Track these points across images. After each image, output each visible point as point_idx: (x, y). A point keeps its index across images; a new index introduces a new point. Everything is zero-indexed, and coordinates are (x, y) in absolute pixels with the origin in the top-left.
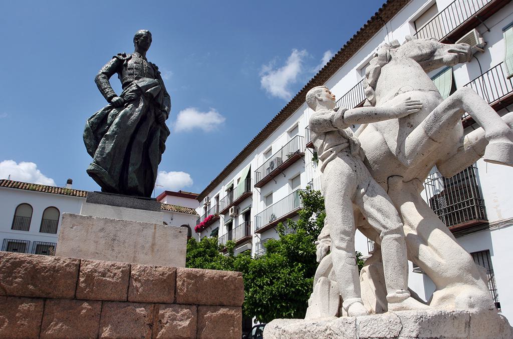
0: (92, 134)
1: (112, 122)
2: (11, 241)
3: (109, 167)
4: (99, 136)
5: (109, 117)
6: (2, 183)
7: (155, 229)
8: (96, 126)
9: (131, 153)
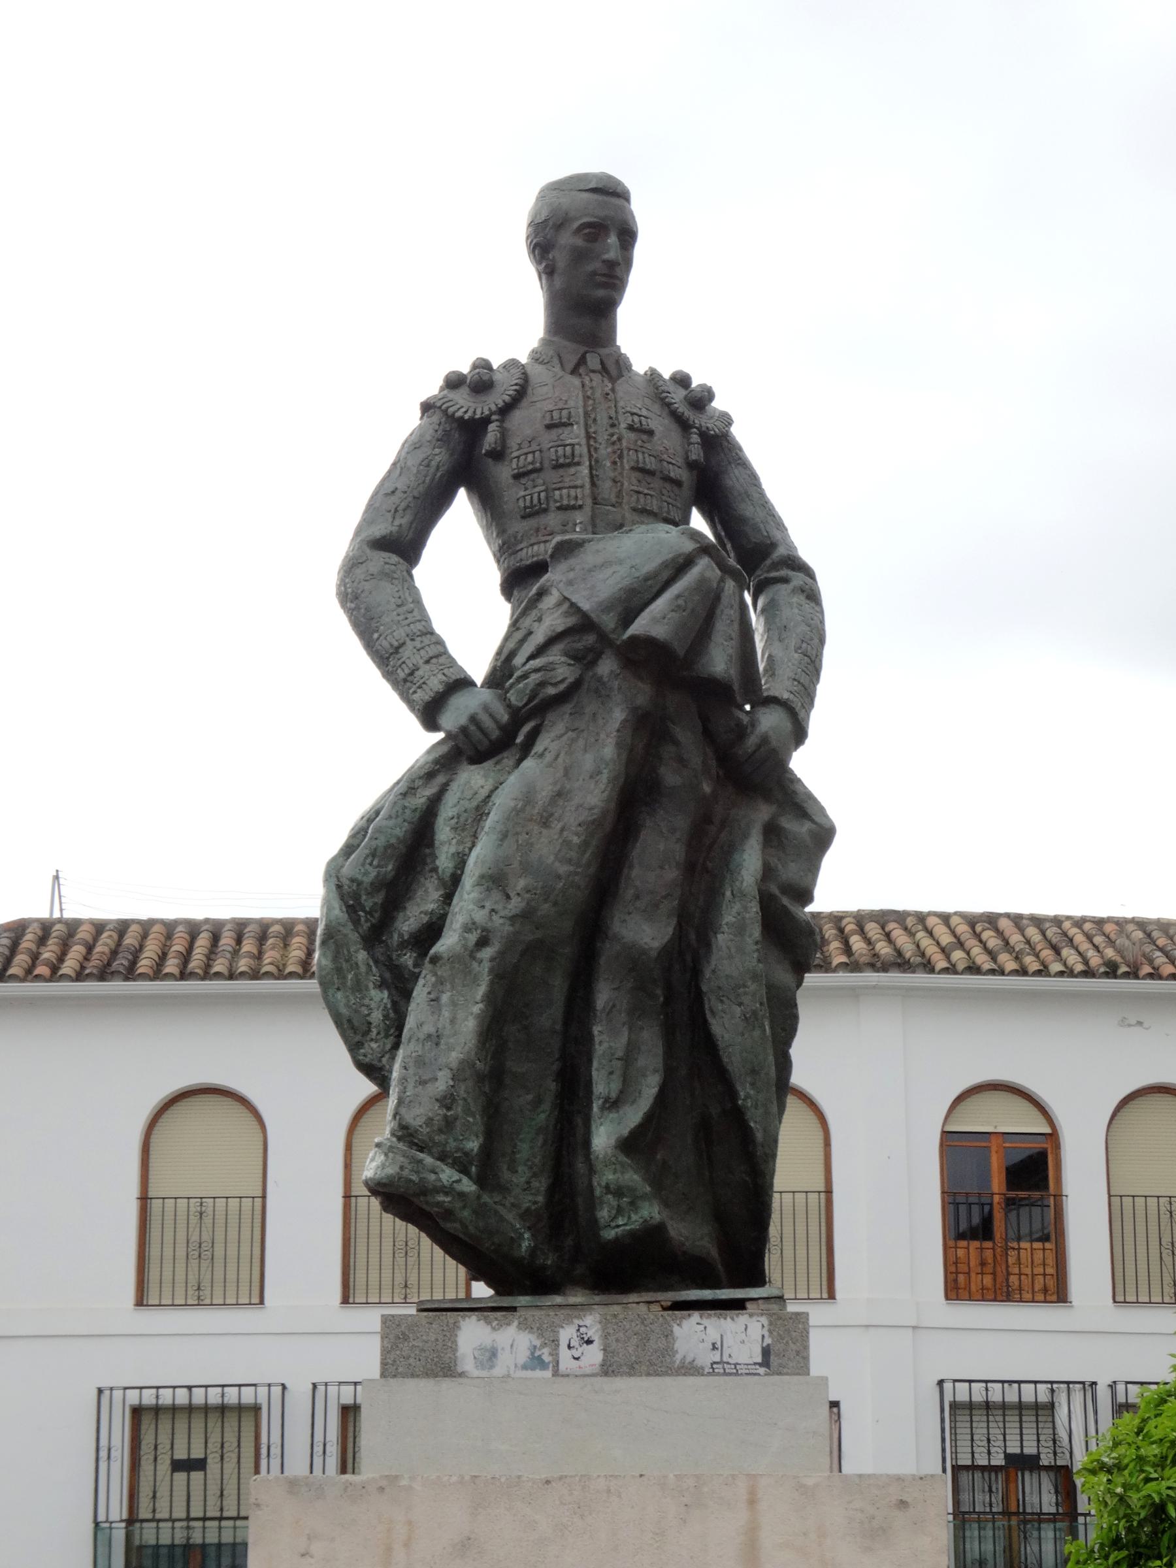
0: (362, 956)
1: (461, 861)
2: (148, 1398)
3: (473, 1145)
4: (408, 959)
5: (443, 832)
6: (14, 948)
7: (752, 1502)
8: (379, 898)
9: (596, 1029)
